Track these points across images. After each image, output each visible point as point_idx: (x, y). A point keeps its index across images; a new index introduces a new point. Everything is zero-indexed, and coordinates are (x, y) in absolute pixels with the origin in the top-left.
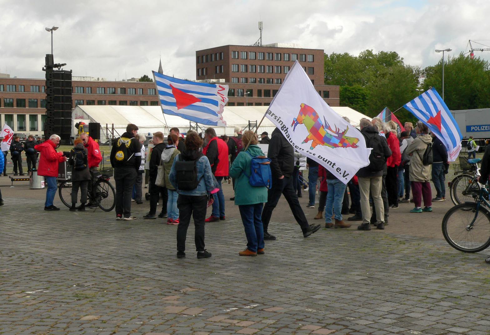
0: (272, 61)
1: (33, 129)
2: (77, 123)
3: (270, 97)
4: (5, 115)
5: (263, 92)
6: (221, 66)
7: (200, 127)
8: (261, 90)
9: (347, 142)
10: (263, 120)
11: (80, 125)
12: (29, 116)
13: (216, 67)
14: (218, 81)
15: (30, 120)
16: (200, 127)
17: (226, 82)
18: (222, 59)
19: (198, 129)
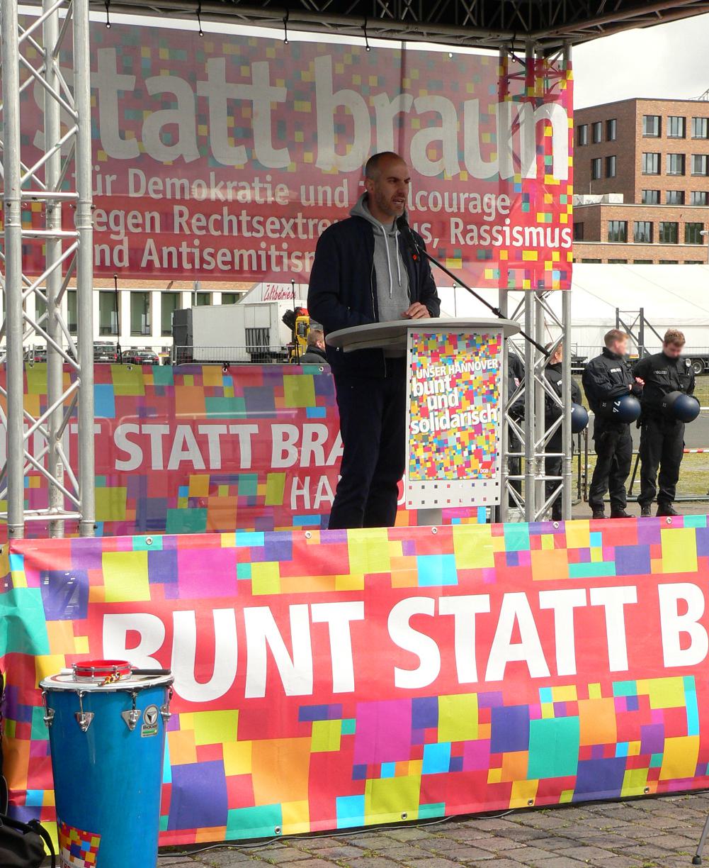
0: (659, 140)
1: (106, 331)
2: (289, 312)
3: (600, 240)
4: (132, 292)
5: (657, 229)
6: (608, 160)
7: (651, 327)
8: (677, 224)
9: (178, 376)
10: (515, 310)
11: (299, 318)
12: (128, 294)
13: (594, 161)
14: (603, 198)
15: (68, 309)
16: (651, 327)
17: (625, 202)
18: (614, 138)
19: (645, 329)
